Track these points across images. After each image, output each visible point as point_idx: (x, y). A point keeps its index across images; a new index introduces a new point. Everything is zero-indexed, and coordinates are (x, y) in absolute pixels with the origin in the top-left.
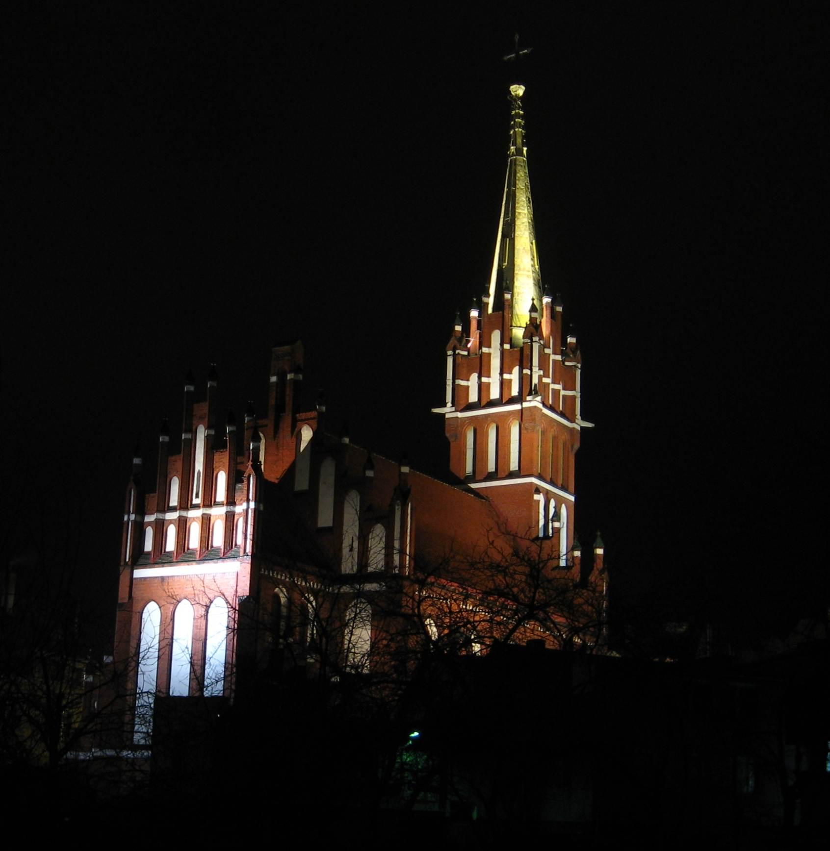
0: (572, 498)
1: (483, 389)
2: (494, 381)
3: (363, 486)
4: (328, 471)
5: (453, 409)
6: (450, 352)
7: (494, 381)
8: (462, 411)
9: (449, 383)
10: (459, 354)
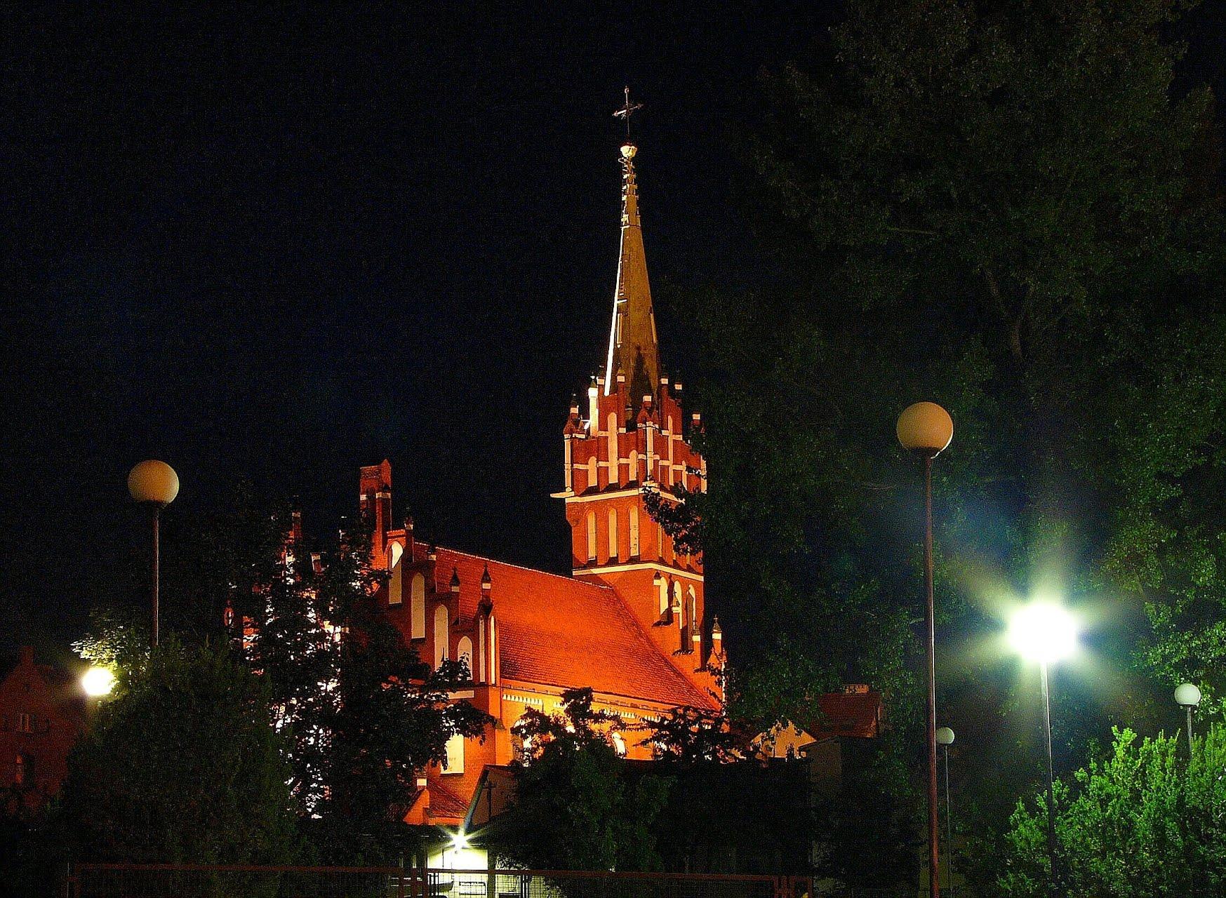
0: (701, 578)
1: (603, 473)
2: (613, 463)
3: (449, 600)
4: (418, 583)
5: (573, 494)
6: (566, 436)
7: (613, 463)
8: (581, 495)
9: (567, 466)
10: (575, 437)
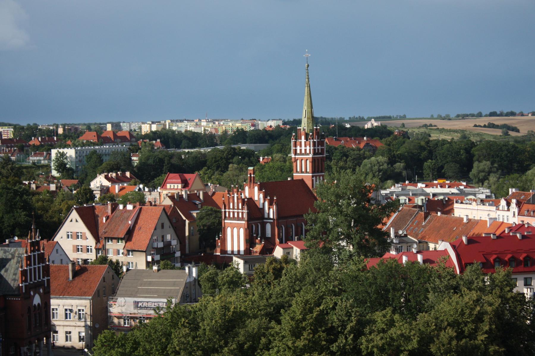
1: (301, 150)
